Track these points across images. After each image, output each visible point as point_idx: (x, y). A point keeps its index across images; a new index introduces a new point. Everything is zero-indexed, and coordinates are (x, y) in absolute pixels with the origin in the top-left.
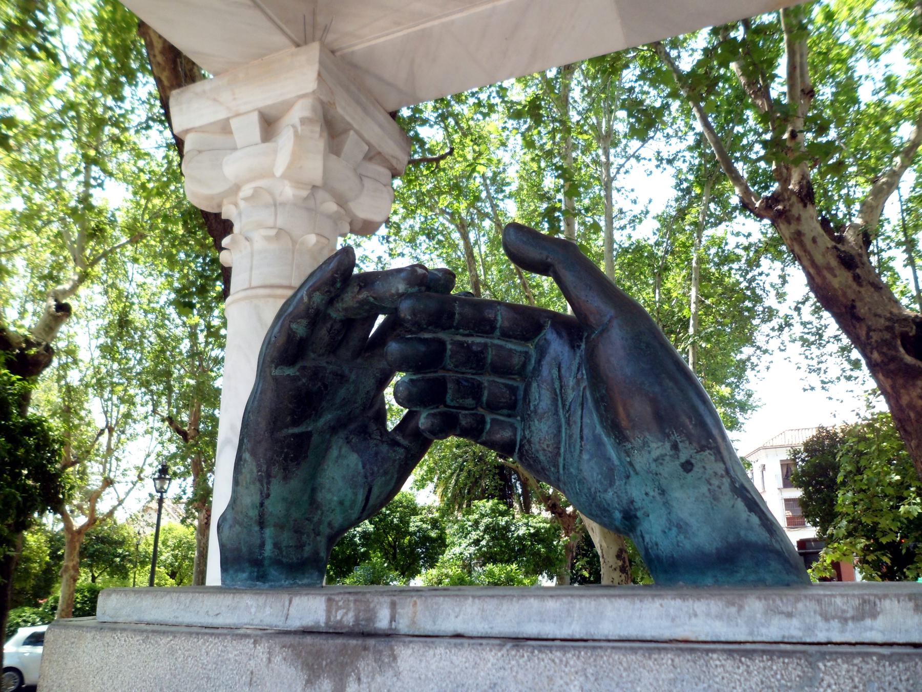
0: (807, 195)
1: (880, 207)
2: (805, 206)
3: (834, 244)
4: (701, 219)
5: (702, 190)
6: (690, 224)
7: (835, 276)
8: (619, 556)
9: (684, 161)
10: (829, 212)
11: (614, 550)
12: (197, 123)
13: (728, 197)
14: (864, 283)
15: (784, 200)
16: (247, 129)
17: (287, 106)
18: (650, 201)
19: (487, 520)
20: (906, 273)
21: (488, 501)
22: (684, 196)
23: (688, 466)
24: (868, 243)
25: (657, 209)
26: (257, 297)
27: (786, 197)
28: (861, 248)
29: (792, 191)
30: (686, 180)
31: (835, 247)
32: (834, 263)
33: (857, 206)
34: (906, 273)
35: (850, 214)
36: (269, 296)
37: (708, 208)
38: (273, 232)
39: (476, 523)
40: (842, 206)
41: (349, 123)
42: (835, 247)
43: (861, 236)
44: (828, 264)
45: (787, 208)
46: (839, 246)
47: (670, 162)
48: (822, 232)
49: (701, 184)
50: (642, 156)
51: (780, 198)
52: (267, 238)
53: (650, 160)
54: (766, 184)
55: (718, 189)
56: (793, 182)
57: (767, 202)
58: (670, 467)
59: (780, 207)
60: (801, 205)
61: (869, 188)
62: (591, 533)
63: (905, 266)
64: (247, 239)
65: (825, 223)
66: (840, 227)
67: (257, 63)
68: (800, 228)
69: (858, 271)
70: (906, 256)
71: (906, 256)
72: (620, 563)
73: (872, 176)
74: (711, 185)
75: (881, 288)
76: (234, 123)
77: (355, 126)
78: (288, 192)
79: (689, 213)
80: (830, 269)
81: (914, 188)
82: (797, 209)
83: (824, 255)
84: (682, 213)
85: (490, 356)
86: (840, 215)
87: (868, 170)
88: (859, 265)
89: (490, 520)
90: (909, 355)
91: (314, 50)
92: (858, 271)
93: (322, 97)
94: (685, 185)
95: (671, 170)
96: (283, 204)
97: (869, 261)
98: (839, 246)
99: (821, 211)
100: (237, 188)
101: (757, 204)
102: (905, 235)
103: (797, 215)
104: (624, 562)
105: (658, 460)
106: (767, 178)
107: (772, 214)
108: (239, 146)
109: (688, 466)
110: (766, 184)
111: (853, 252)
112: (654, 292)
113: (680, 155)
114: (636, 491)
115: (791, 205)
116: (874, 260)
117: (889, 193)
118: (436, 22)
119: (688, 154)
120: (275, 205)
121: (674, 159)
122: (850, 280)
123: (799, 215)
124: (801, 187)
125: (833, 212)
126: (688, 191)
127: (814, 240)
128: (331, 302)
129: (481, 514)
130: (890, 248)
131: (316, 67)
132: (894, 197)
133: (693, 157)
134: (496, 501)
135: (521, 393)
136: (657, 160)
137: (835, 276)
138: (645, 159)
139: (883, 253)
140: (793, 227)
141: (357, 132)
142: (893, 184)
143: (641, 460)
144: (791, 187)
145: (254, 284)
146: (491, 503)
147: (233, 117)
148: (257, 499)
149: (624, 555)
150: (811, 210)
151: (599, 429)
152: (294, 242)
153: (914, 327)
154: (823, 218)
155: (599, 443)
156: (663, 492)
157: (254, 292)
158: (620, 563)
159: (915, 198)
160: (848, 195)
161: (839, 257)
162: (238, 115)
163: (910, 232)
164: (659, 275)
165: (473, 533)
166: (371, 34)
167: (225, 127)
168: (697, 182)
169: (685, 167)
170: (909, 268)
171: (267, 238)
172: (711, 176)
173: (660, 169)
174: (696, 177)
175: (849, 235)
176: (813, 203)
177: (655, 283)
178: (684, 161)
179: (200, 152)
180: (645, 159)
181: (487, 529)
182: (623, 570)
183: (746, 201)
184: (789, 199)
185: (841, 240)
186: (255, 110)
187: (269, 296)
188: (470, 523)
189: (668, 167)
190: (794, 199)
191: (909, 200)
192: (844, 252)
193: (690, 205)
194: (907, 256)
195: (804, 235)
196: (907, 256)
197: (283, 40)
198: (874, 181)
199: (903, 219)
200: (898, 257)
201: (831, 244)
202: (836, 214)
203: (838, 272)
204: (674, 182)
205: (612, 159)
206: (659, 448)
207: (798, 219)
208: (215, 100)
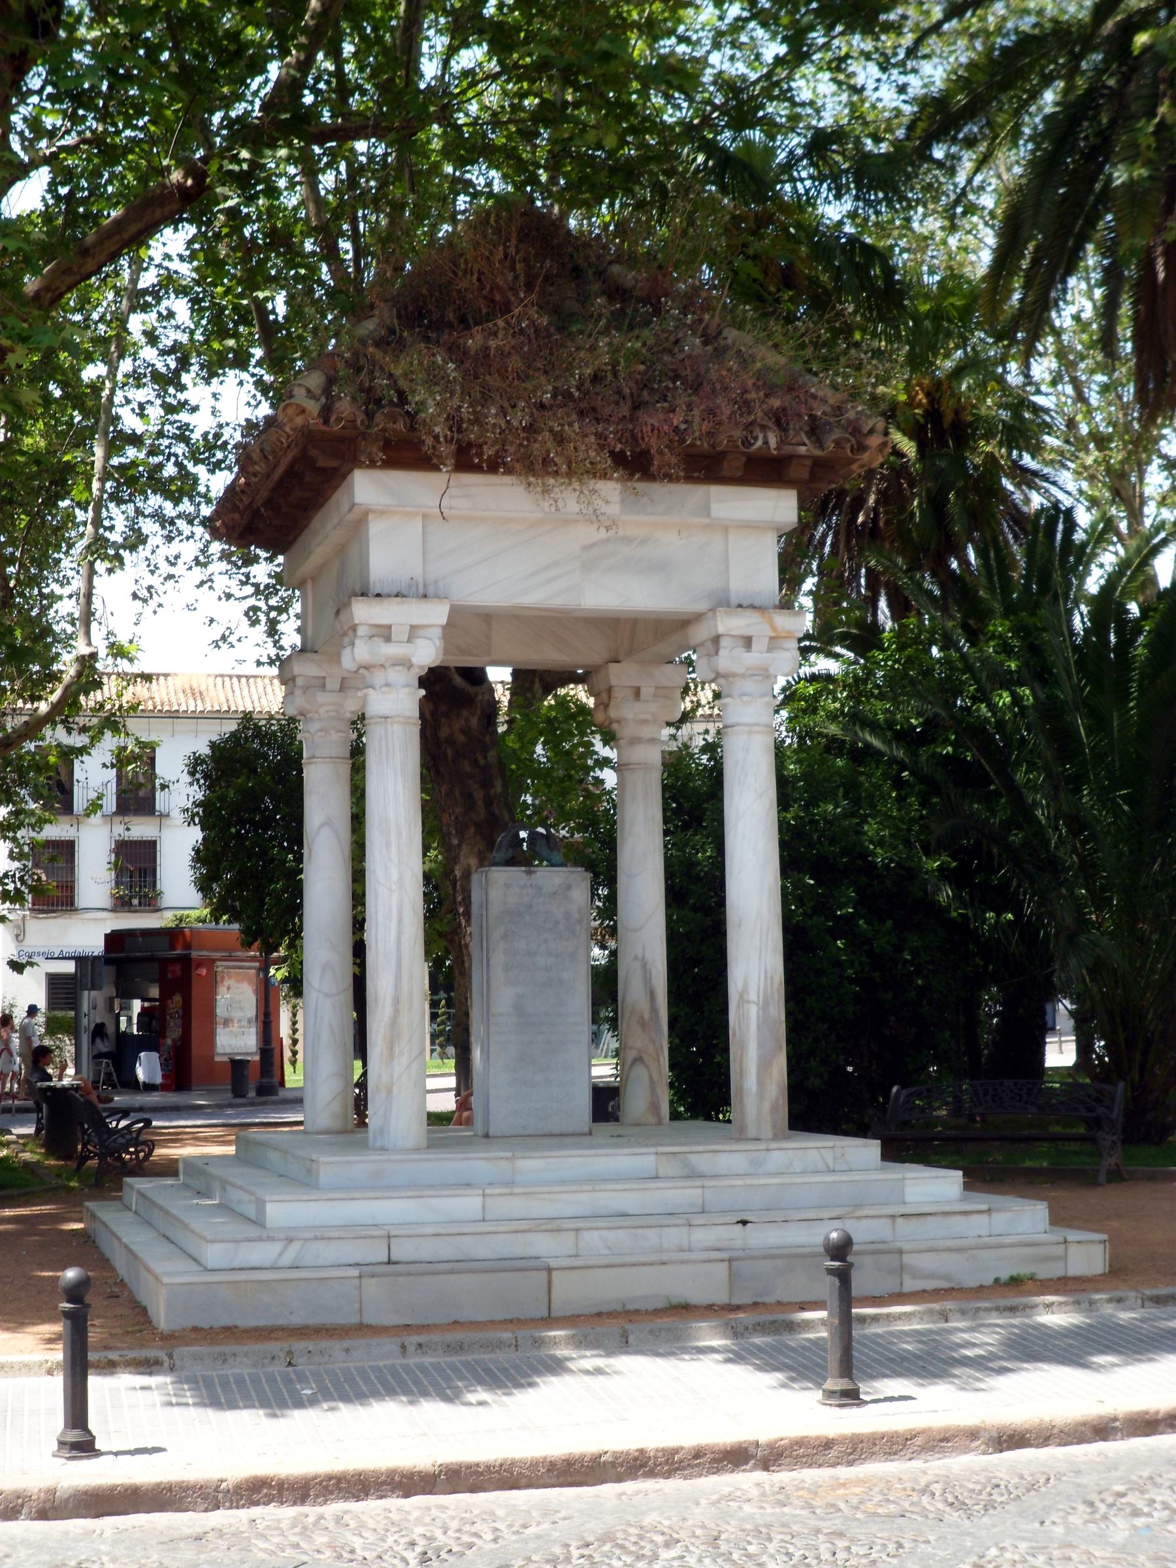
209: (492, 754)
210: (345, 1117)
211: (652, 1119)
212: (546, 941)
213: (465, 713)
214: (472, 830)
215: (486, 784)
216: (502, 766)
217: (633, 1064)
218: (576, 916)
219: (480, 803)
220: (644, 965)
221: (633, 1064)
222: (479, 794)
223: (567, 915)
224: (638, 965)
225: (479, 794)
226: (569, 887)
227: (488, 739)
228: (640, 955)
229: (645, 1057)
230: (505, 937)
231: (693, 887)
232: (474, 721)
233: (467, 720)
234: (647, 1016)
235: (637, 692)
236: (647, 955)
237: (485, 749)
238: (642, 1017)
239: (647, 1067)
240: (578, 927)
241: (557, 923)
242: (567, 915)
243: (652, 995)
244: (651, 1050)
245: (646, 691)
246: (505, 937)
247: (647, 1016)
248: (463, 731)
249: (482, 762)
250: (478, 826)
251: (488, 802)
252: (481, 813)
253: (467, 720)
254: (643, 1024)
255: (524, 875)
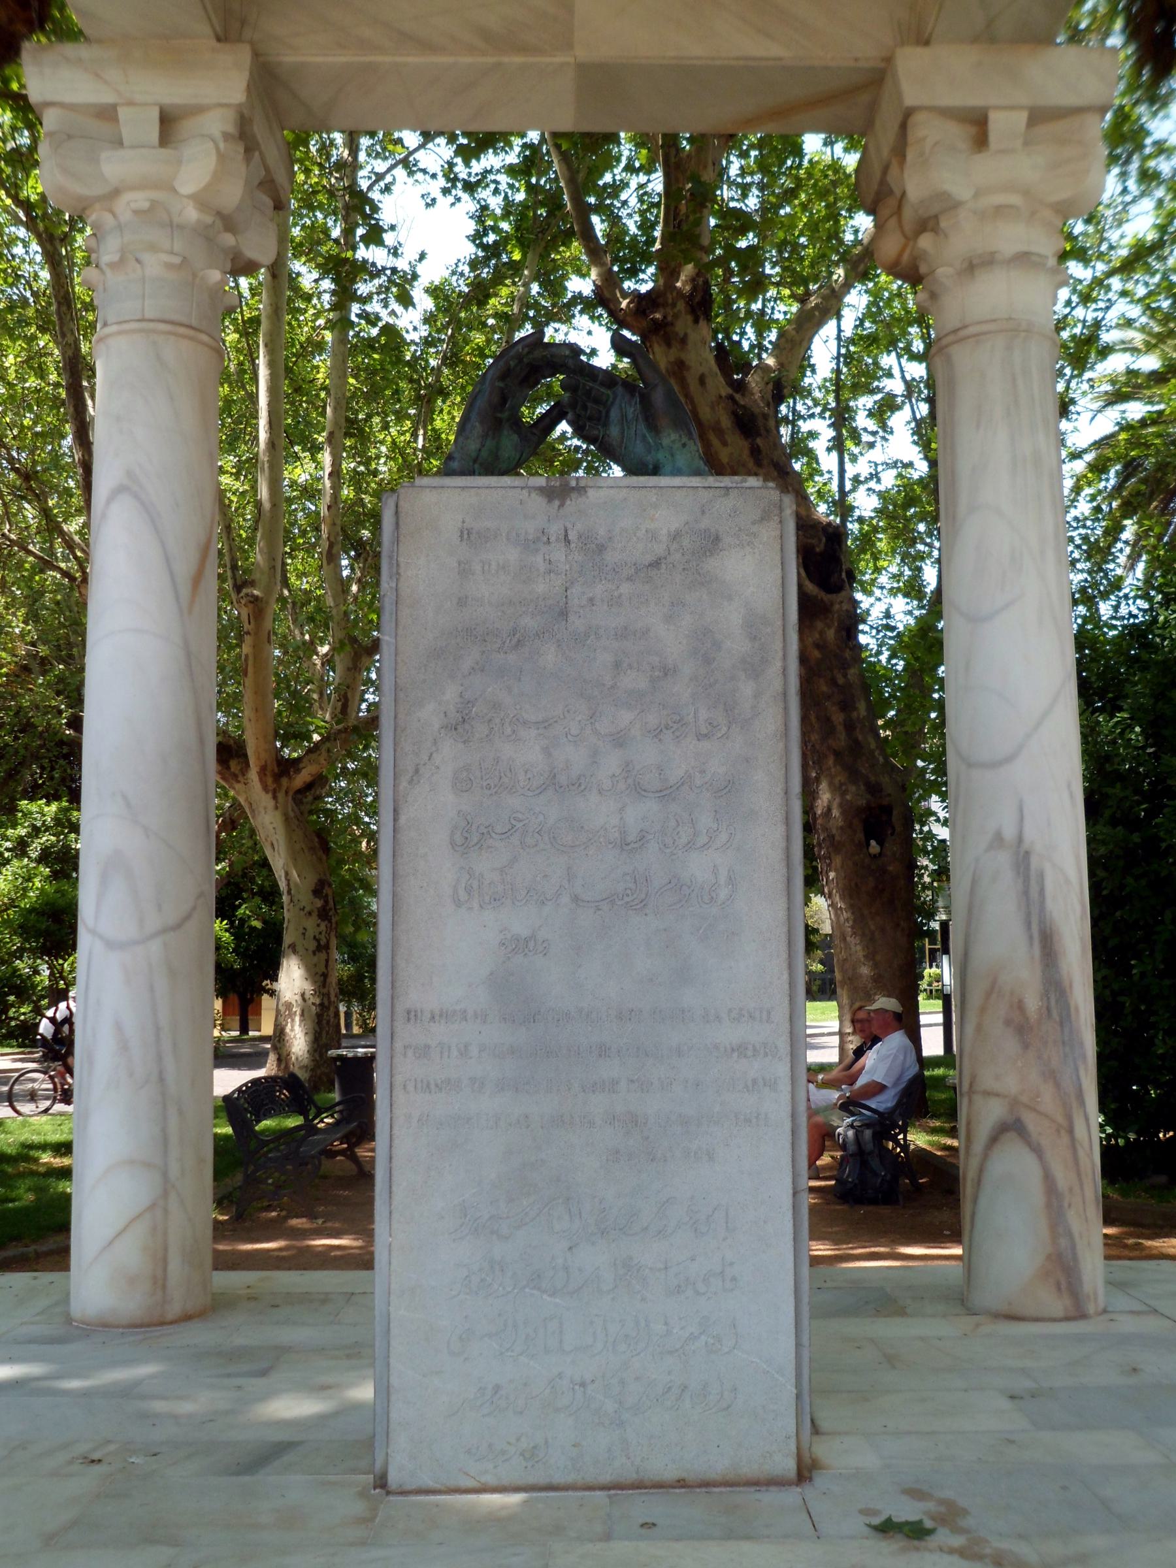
0: (701, 304)
1: (805, 344)
2: (696, 321)
3: (730, 391)
4: (516, 309)
5: (524, 255)
6: (496, 315)
7: (725, 444)
8: (317, 892)
9: (496, 192)
10: (728, 337)
11: (311, 880)
12: (68, 98)
13: (565, 277)
14: (765, 462)
15: (665, 305)
16: (140, 125)
17: (198, 110)
18: (422, 256)
19: (47, 838)
20: (828, 461)
21: (48, 804)
22: (487, 259)
23: (684, 445)
24: (779, 399)
25: (432, 273)
26: (154, 331)
27: (670, 301)
28: (768, 405)
29: (679, 291)
30: (495, 229)
31: (731, 398)
32: (726, 422)
33: (773, 336)
34: (828, 461)
35: (761, 347)
36: (170, 333)
37: (528, 290)
38: (177, 260)
39: (21, 847)
40: (750, 331)
41: (258, 144)
42: (731, 398)
43: (770, 386)
44: (718, 422)
45: (669, 318)
46: (737, 397)
47: (470, 187)
48: (715, 368)
49: (524, 245)
50: (421, 165)
51: (661, 300)
52: (169, 266)
53: (434, 176)
54: (634, 265)
55: (554, 260)
56: (683, 277)
57: (639, 303)
58: (678, 445)
59: (658, 316)
60: (689, 318)
61: (795, 308)
62: (268, 853)
63: (829, 450)
64: (138, 260)
65: (722, 354)
66: (746, 367)
67: (163, 48)
68: (683, 356)
69: (759, 441)
70: (831, 433)
71: (831, 433)
72: (319, 903)
73: (801, 291)
74: (540, 250)
75: (788, 473)
76: (123, 113)
77: (263, 147)
78: (192, 214)
79: (496, 295)
80: (719, 432)
81: (862, 321)
82: (684, 323)
83: (712, 408)
84: (480, 292)
85: (593, 393)
86: (746, 345)
87: (793, 278)
88: (763, 432)
89: (53, 838)
90: (811, 580)
91: (244, 55)
92: (759, 441)
93: (245, 111)
94: (491, 238)
95: (468, 205)
96: (181, 227)
97: (778, 432)
98: (737, 397)
99: (716, 332)
100: (116, 193)
101: (624, 304)
102: (837, 399)
103: (681, 335)
104: (326, 902)
105: (673, 442)
106: (638, 254)
107: (644, 324)
108: (126, 142)
109: (684, 445)
110: (634, 265)
111: (756, 411)
112: (415, 435)
113: (491, 177)
114: (660, 456)
115: (676, 316)
116: (785, 432)
117: (820, 324)
118: (388, 59)
119: (504, 179)
120: (172, 226)
121: (478, 183)
122: (746, 452)
123: (686, 335)
124: (694, 288)
125: (736, 338)
126: (493, 251)
127: (702, 380)
128: (529, 353)
129: (34, 827)
130: (812, 416)
131: (246, 75)
132: (829, 329)
133: (511, 186)
134: (65, 804)
135: (604, 414)
136: (448, 180)
137: (725, 444)
138: (424, 171)
139: (800, 423)
140: (674, 354)
141: (261, 153)
142: (831, 307)
143: (666, 442)
144: (679, 284)
145: (148, 315)
146: (54, 807)
147: (123, 104)
148: (478, 446)
149: (327, 890)
150: (704, 329)
151: (645, 431)
152: (194, 275)
153: (824, 539)
154: (720, 346)
155: (644, 436)
156: (672, 455)
157: (151, 325)
158: (319, 903)
159: (861, 337)
160: (762, 312)
161: (735, 414)
162: (130, 103)
163: (846, 394)
164: (428, 401)
165: (15, 862)
166: (308, 51)
167: (107, 113)
168: (518, 239)
169: (496, 204)
170: (834, 455)
171: (169, 266)
172: (543, 232)
173: (451, 199)
174: (517, 228)
175: (753, 380)
176: (709, 319)
177: (418, 415)
178: (496, 192)
179: (70, 137)
180: (424, 171)
181: (45, 857)
182: (324, 914)
183: (607, 294)
184: (674, 305)
185: (740, 387)
186: (155, 104)
187: (170, 333)
188: (8, 844)
189: (465, 197)
190: (681, 305)
191: (851, 341)
192: (744, 407)
193: (498, 278)
194: (834, 434)
195: (688, 368)
196: (834, 434)
197: (207, 30)
198: (802, 300)
199: (838, 372)
200: (822, 429)
201: (725, 391)
202: (739, 343)
203: (729, 438)
204: (471, 227)
205: (362, 157)
206: (674, 436)
207: (683, 341)
208: (97, 75)
209: (852, 672)
210: (160, 1281)
211: (1057, 1305)
212: (620, 740)
213: (819, 625)
214: (831, 761)
215: (846, 706)
216: (866, 688)
217: (994, 1140)
218: (737, 645)
219: (840, 728)
220: (1023, 861)
221: (994, 1140)
222: (838, 718)
223: (705, 645)
224: (1003, 860)
225: (838, 718)
226: (712, 543)
227: (848, 654)
228: (1009, 833)
229: (1030, 1121)
230: (459, 724)
231: (1110, 791)
232: (831, 634)
233: (821, 633)
234: (1033, 1004)
235: (978, 128)
236: (1030, 834)
237: (844, 666)
238: (1020, 1006)
239: (1037, 1151)
240: (747, 689)
241: (667, 672)
242: (705, 645)
243: (1048, 945)
244: (1048, 1100)
245: (1005, 124)
246: (459, 724)
247: (1033, 1004)
248: (817, 646)
249: (841, 681)
250: (837, 754)
251: (850, 727)
252: (841, 739)
253: (821, 633)
254: (1022, 1028)
255: (537, 502)
